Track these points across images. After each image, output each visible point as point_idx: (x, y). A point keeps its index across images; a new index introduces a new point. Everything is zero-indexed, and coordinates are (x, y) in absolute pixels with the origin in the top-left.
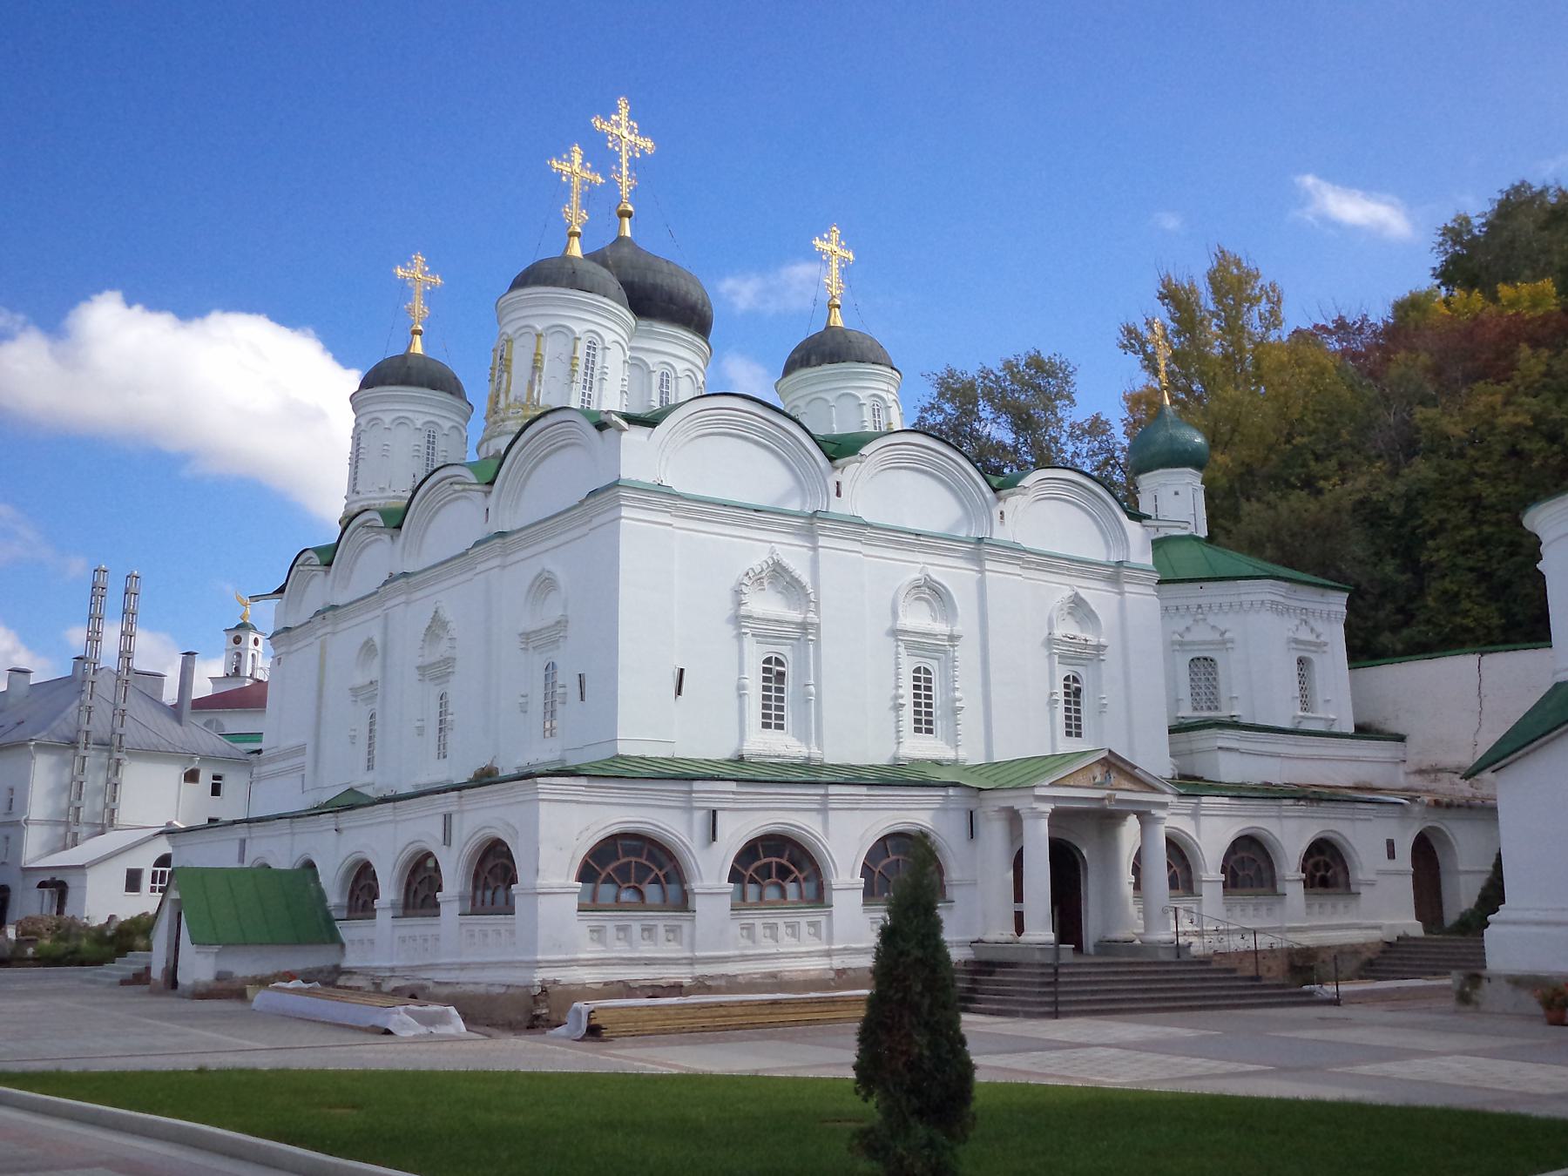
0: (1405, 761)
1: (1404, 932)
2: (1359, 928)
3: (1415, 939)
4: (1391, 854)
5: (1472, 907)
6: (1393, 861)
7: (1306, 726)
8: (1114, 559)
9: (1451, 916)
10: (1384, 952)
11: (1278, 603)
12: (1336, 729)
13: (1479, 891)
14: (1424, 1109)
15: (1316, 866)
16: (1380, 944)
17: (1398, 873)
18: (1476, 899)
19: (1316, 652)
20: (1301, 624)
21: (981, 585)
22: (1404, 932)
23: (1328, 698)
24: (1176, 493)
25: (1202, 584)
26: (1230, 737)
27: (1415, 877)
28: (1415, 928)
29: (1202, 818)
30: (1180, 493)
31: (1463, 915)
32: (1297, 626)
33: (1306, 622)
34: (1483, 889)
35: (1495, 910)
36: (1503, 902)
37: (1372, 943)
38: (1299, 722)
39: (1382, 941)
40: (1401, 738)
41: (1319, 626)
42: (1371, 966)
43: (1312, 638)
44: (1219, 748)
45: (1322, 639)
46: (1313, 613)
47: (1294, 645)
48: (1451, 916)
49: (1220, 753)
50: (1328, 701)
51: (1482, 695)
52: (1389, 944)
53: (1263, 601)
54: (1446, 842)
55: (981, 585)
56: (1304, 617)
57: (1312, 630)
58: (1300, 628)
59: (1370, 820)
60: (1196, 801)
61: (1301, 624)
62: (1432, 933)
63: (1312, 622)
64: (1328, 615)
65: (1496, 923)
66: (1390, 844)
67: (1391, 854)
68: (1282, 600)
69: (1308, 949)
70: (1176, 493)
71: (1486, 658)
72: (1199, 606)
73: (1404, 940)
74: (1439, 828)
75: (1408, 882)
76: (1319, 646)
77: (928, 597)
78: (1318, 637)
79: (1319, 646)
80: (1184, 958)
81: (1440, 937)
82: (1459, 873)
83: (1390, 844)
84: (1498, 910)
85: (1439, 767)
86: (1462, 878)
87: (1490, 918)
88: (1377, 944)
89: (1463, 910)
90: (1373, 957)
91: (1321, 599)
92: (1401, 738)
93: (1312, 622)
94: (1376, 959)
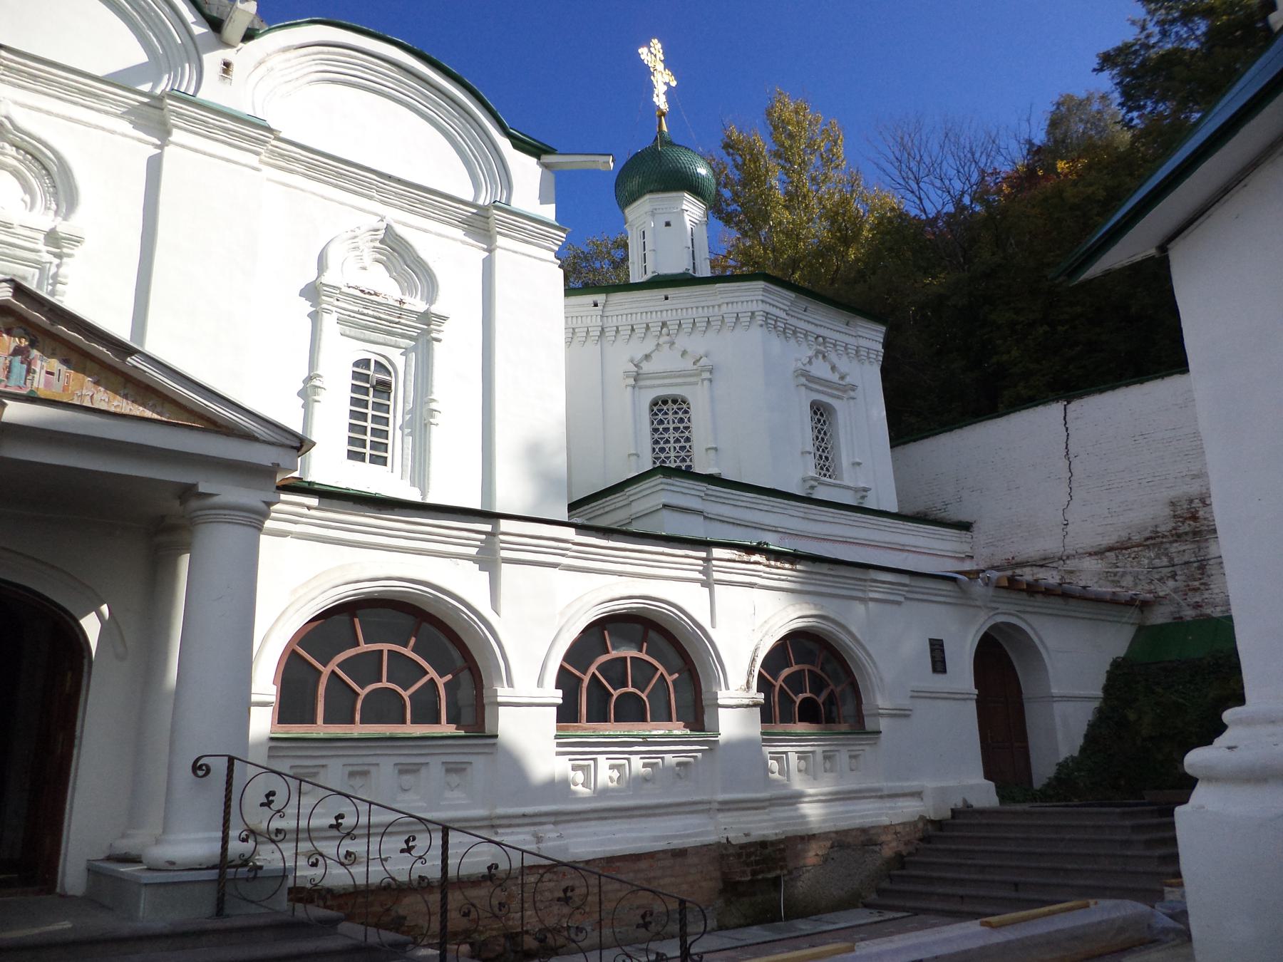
0: (972, 557)
1: (965, 801)
2: (881, 797)
3: (982, 812)
4: (939, 664)
5: (1076, 754)
6: (941, 676)
7: (821, 494)
8: (484, 200)
9: (1043, 770)
10: (925, 839)
11: (777, 318)
12: (871, 503)
13: (1083, 728)
14: (1088, 394)
15: (795, 682)
16: (920, 825)
17: (952, 696)
18: (1080, 741)
19: (839, 397)
20: (816, 356)
21: (154, 167)
22: (965, 801)
23: (858, 460)
24: (668, 224)
25: (670, 292)
26: (686, 491)
27: (982, 704)
28: (983, 794)
29: (505, 568)
30: (672, 223)
31: (1061, 766)
32: (810, 359)
33: (824, 357)
34: (1092, 726)
35: (1211, 730)
36: (1240, 700)
37: (904, 824)
38: (812, 487)
39: (922, 818)
40: (965, 526)
41: (844, 364)
42: (903, 867)
43: (835, 378)
44: (665, 506)
45: (848, 380)
46: (835, 345)
47: (803, 380)
48: (1043, 770)
49: (666, 513)
50: (859, 464)
51: (1071, 456)
52: (939, 824)
53: (753, 313)
54: (1030, 649)
55: (154, 167)
56: (821, 348)
57: (833, 368)
58: (814, 360)
59: (899, 603)
60: (488, 528)
61: (816, 356)
62: (1014, 800)
63: (833, 356)
64: (857, 352)
65: (1213, 778)
66: (937, 648)
67: (939, 664)
68: (783, 315)
69: (763, 844)
70: (668, 224)
71: (1075, 406)
72: (664, 324)
73: (963, 815)
74: (1014, 625)
75: (970, 711)
76: (846, 389)
77: (15, 163)
78: (842, 378)
79: (846, 389)
80: (241, 914)
81: (1025, 807)
82: (1052, 698)
83: (937, 648)
84: (1221, 728)
85: (1018, 559)
86: (1058, 708)
87: (1195, 759)
88: (914, 824)
89: (1061, 759)
90: (904, 850)
91: (843, 328)
92: (965, 526)
93: (833, 356)
94: (910, 854)
